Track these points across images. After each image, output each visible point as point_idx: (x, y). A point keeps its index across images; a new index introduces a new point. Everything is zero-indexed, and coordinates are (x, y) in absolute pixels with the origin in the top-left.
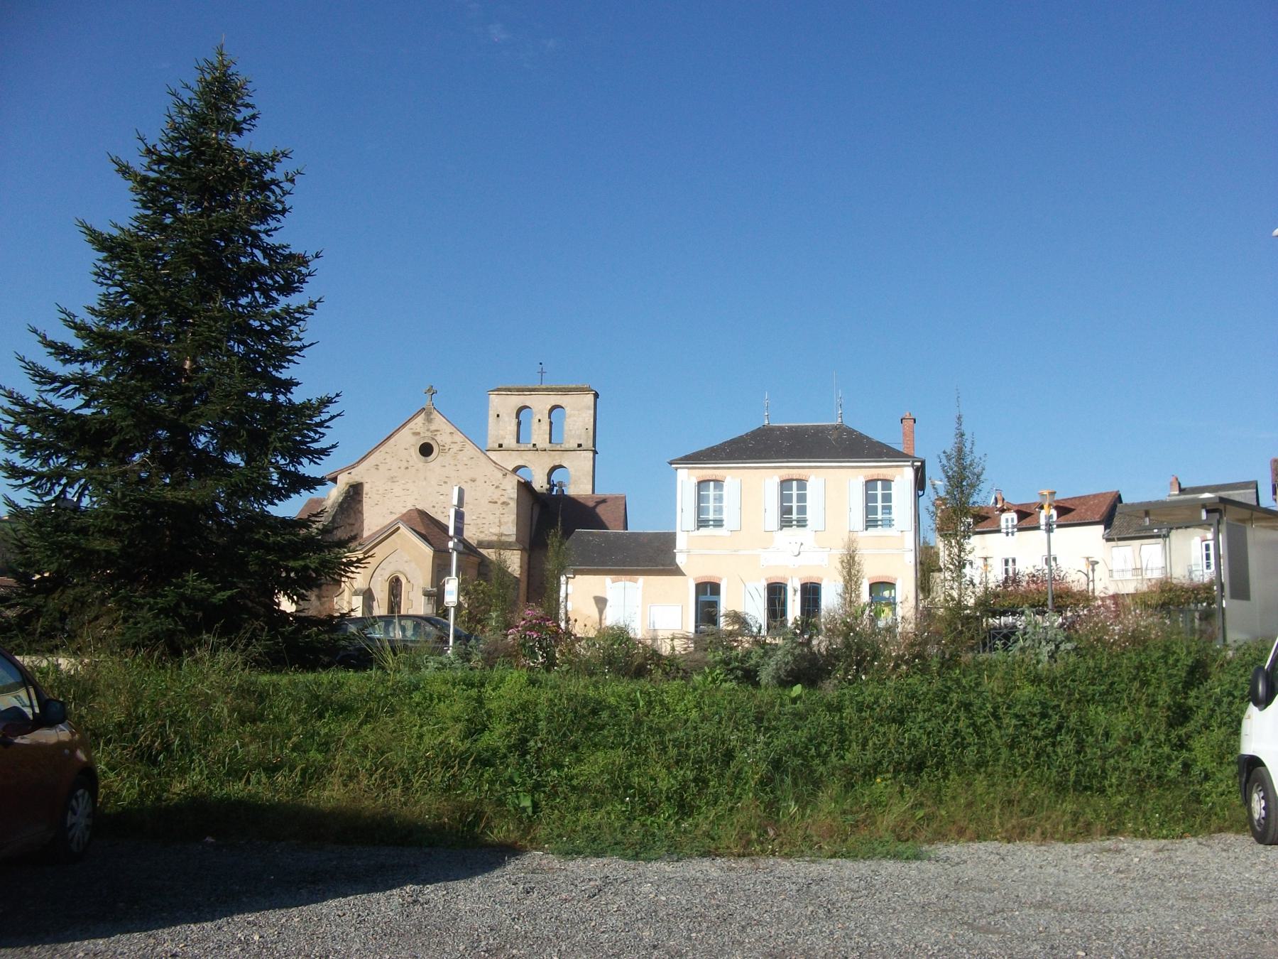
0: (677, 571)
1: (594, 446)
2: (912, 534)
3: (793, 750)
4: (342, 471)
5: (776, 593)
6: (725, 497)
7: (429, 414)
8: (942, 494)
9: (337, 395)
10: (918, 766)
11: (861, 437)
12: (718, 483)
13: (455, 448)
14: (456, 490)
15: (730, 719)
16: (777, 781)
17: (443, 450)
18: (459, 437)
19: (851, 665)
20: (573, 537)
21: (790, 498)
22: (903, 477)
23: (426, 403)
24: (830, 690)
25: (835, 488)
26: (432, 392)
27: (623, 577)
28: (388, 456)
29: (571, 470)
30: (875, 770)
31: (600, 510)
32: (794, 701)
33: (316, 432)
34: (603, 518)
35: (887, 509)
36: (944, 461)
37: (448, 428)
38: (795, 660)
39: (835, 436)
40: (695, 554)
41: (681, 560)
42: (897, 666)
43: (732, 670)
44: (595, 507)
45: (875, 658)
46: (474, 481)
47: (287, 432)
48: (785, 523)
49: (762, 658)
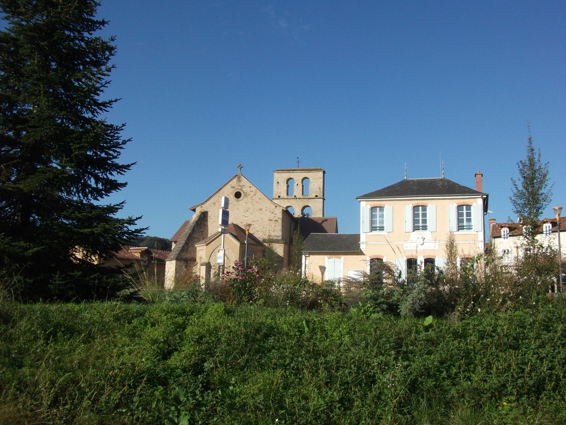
0: (361, 253)
1: (323, 196)
2: (482, 233)
3: (427, 373)
4: (198, 206)
5: (411, 263)
6: (385, 222)
7: (239, 178)
8: (520, 188)
9: (123, 125)
10: (539, 388)
11: (454, 184)
12: (382, 208)
13: (252, 194)
14: (223, 198)
15: (374, 344)
16: (414, 402)
17: (246, 195)
18: (254, 189)
19: (469, 301)
20: (309, 236)
21: (418, 215)
22: (477, 204)
23: (238, 173)
24: (454, 320)
25: (442, 211)
26: (241, 167)
27: (334, 256)
29: (313, 208)
30: (500, 393)
31: (324, 225)
32: (427, 329)
33: (115, 151)
34: (326, 228)
35: (469, 220)
36: (521, 167)
38: (426, 297)
39: (441, 184)
40: (371, 244)
41: (363, 247)
42: (504, 302)
43: (379, 304)
44: (322, 223)
45: (486, 296)
47: (95, 153)
48: (416, 228)
49: (401, 295)
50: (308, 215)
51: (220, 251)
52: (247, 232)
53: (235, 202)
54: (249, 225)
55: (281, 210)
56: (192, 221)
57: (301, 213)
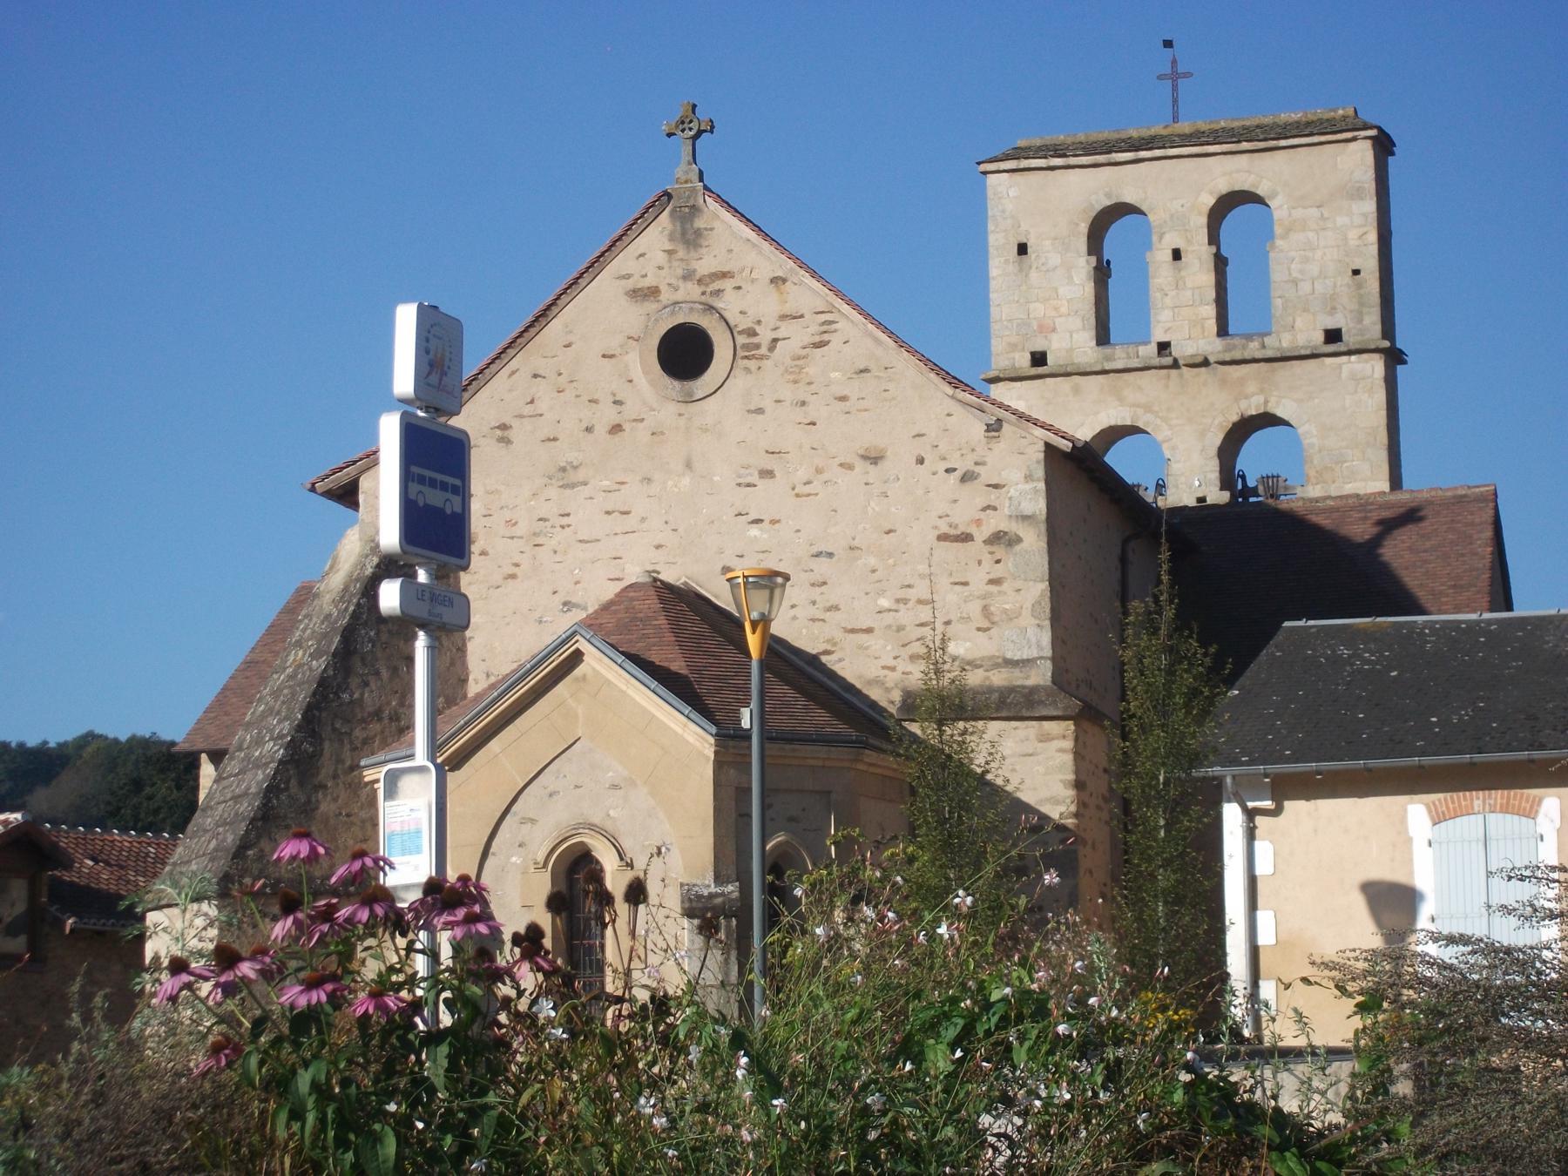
1: (1388, 329)
13: (797, 336)
14: (406, 319)
17: (749, 348)
18: (808, 294)
20: (1271, 651)
26: (694, 127)
27: (1478, 799)
28: (542, 389)
29: (1308, 430)
31: (1397, 552)
37: (764, 260)
44: (1376, 542)
46: (874, 459)
50: (1272, 484)
51: (407, 784)
52: (753, 641)
53: (668, 413)
54: (770, 581)
55: (1037, 454)
56: (337, 581)
57: (1214, 476)
